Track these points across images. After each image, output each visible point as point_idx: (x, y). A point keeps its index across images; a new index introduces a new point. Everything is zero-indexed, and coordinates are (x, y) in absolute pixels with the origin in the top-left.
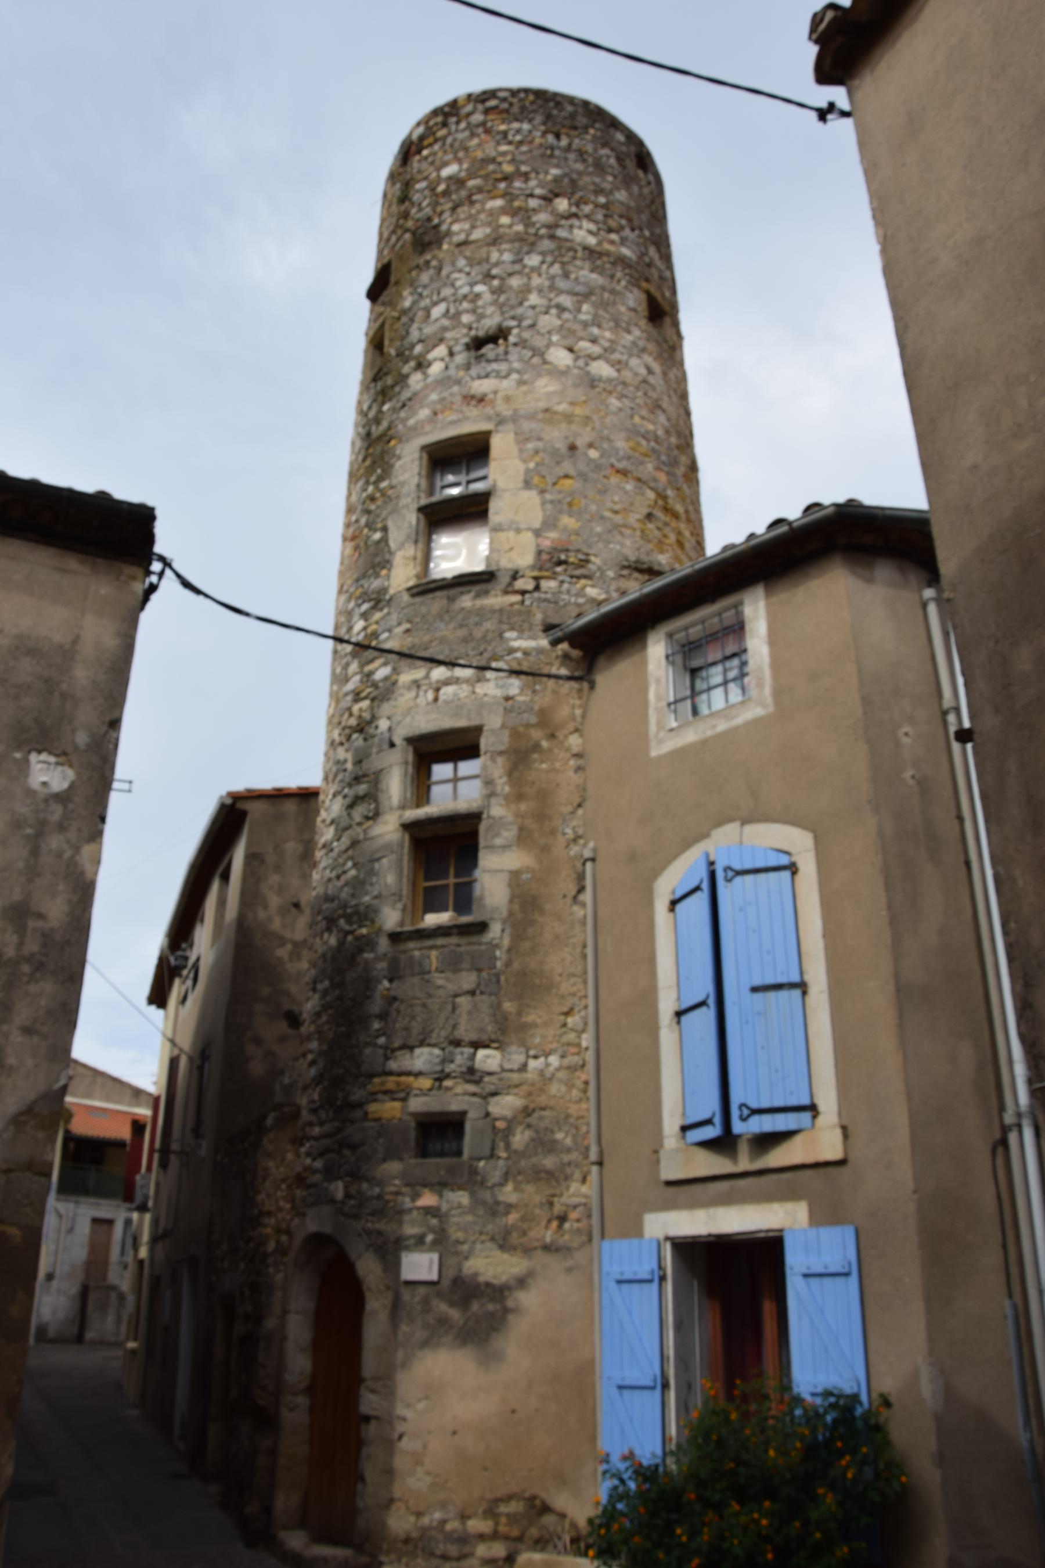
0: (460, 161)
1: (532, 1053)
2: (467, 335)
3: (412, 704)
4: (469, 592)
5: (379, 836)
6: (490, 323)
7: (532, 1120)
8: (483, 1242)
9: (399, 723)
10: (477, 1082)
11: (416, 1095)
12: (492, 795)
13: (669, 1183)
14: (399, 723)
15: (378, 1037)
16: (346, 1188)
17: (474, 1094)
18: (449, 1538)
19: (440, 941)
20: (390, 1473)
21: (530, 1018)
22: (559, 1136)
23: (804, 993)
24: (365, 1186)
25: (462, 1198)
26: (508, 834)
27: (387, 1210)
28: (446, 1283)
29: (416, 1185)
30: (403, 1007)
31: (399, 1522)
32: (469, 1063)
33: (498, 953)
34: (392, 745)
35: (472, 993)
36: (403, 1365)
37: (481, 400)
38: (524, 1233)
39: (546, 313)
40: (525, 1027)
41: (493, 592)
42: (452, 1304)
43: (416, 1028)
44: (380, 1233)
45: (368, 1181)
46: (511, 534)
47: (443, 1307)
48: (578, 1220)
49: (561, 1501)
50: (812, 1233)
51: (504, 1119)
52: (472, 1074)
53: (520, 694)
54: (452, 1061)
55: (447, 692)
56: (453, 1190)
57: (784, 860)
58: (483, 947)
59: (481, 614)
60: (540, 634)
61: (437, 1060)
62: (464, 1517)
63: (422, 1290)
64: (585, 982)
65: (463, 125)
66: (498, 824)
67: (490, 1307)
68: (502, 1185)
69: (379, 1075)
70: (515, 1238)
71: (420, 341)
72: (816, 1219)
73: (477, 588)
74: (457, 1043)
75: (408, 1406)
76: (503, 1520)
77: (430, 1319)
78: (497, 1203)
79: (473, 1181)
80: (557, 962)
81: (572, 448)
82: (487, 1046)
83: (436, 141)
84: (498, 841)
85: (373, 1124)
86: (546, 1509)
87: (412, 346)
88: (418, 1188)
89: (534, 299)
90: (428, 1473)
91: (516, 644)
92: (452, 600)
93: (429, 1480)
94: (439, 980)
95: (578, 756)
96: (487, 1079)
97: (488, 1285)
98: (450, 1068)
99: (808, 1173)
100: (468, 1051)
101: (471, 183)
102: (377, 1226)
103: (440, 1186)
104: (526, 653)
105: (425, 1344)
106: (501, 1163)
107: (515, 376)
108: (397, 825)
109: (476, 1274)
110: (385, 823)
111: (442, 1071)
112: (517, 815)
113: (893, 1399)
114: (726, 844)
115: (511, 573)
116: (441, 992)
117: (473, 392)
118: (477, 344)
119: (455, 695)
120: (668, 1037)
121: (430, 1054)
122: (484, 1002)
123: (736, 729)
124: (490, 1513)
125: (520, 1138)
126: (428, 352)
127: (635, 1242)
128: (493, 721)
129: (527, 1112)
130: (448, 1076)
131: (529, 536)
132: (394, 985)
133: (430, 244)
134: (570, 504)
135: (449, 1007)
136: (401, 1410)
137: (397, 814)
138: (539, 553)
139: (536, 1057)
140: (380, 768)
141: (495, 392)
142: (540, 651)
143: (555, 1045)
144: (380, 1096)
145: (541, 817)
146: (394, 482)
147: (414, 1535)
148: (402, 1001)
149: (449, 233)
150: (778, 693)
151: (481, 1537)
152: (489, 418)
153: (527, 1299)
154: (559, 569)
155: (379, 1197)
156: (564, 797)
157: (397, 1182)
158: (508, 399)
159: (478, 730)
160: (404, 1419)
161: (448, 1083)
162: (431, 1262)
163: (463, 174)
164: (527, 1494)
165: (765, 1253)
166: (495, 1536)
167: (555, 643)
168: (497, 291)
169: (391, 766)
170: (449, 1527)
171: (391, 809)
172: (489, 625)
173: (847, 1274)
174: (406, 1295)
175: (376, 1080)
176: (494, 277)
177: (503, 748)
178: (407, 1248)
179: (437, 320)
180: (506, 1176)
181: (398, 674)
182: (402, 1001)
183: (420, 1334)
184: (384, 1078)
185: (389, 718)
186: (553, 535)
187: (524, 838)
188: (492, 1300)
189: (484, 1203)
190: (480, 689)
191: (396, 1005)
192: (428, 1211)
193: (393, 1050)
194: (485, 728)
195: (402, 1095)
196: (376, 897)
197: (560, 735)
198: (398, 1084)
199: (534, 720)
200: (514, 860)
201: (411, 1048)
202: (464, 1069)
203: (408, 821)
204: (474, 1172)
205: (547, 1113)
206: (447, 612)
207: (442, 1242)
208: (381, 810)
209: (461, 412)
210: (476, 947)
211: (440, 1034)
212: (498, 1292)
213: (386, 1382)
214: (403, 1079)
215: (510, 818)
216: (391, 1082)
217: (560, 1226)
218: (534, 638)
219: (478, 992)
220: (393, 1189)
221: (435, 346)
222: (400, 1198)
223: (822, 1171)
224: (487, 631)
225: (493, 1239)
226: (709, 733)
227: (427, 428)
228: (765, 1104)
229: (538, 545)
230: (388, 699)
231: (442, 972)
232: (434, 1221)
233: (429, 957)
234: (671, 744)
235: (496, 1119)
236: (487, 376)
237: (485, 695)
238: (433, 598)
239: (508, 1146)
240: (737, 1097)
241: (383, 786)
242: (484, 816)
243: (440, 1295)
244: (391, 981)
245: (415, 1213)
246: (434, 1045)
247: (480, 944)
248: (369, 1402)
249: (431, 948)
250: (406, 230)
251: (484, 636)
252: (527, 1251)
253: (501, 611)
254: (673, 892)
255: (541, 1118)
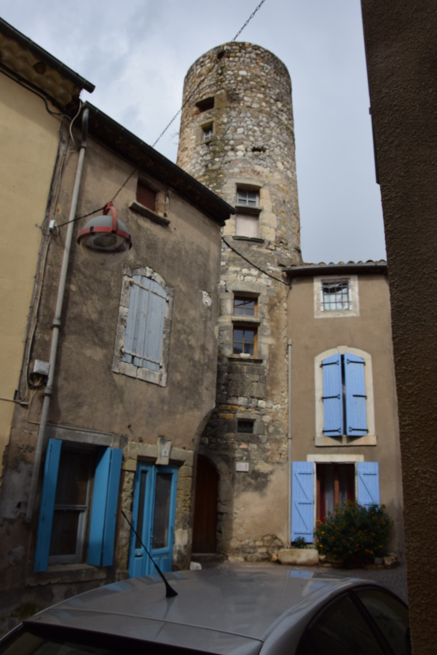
0: (247, 71)
1: (274, 403)
2: (251, 145)
3: (235, 279)
4: (256, 244)
5: (222, 322)
6: (260, 144)
7: (274, 424)
8: (260, 460)
9: (230, 284)
10: (259, 410)
11: (239, 412)
12: (264, 318)
13: (317, 447)
14: (230, 284)
15: (223, 391)
16: (209, 440)
17: (258, 414)
18: (251, 547)
19: (247, 363)
20: (231, 529)
21: (274, 392)
22: (280, 429)
23: (366, 399)
24: (219, 440)
25: (255, 446)
26: (268, 332)
27: (229, 448)
28: (250, 472)
29: (240, 441)
30: (234, 383)
31: (234, 544)
32: (256, 404)
33: (265, 370)
34: (227, 291)
35: (257, 382)
36: (237, 497)
37: (258, 173)
38: (272, 458)
39: (277, 147)
40: (273, 395)
41: (263, 247)
42: (252, 478)
43: (239, 391)
44: (226, 456)
45: (220, 438)
46: (268, 228)
47: (249, 479)
48: (284, 455)
49: (280, 536)
50: (366, 463)
51: (266, 423)
52: (257, 408)
53: (272, 285)
54: (251, 403)
55: (248, 278)
56: (252, 444)
57: (362, 361)
58: (261, 368)
59: (260, 253)
60: (277, 266)
61: (246, 402)
62: (255, 541)
63: (242, 474)
64: (288, 383)
65: (247, 56)
66: (265, 328)
67: (263, 480)
68: (266, 443)
69: (224, 404)
70: (270, 459)
71: (232, 139)
72: (366, 460)
73: (258, 244)
74: (253, 397)
75: (238, 509)
76: (265, 542)
77: (246, 483)
78: (265, 448)
79: (257, 441)
80: (281, 375)
81: (284, 202)
82: (261, 399)
83: (236, 56)
84: (266, 334)
85: (222, 420)
86: (276, 538)
87: (229, 140)
88: (240, 442)
89: (273, 140)
90: (244, 529)
91: (270, 268)
92: (250, 245)
93: (244, 531)
94: (247, 376)
95: (286, 310)
96: (262, 410)
97: (262, 473)
98: (251, 405)
99: (364, 448)
100: (256, 400)
101: (252, 83)
102: (225, 453)
103: (248, 442)
104: (273, 272)
105: (244, 490)
106: (266, 436)
107: (268, 169)
108: (230, 321)
109: (259, 470)
110: (225, 319)
111: (248, 406)
112: (271, 326)
113: (386, 506)
114: (353, 353)
115: (268, 242)
116: (248, 380)
117: (255, 169)
118: (254, 150)
119: (251, 280)
120: (319, 405)
121: (244, 400)
122: (261, 385)
123: (346, 318)
124: (262, 540)
125: (271, 429)
126: (237, 145)
127: (305, 463)
128: (264, 293)
129: (273, 421)
130: (250, 407)
131: (273, 230)
132: (230, 375)
133: (235, 100)
134: (284, 222)
135: (250, 385)
136: (235, 510)
137: (231, 317)
138: (276, 237)
139: (275, 405)
140: (223, 298)
141: (263, 172)
142: (277, 272)
143: (279, 402)
144: (225, 411)
145: (277, 328)
146: (223, 192)
147: (240, 547)
148: (233, 381)
149: (242, 99)
150: (361, 311)
151: (260, 547)
152: (261, 182)
153: (272, 478)
154: (281, 244)
155: (226, 444)
156: (283, 323)
157: (232, 440)
158: (267, 177)
159: (258, 294)
160: (236, 513)
161: (250, 410)
162: (246, 465)
163: (248, 77)
164: (272, 534)
165: (349, 469)
166: (263, 546)
167: (283, 271)
168: (263, 132)
169: (227, 299)
170: (250, 544)
171: (227, 314)
172: (262, 258)
173: (375, 475)
174: (237, 475)
175: (223, 406)
176: (261, 126)
177: (267, 303)
178: (237, 461)
179: (240, 134)
180: (267, 440)
181: (229, 266)
182: (233, 381)
183: (242, 488)
184: (226, 405)
185: (225, 281)
186: (280, 232)
187: (273, 334)
188: (264, 478)
189: (261, 448)
190: (260, 280)
191: (231, 382)
192: (244, 450)
193: (230, 397)
194: (261, 295)
195: (234, 412)
196: (221, 344)
197: (282, 301)
198: (232, 408)
199: (275, 295)
200: (270, 341)
201: (237, 397)
202: (255, 406)
203: (235, 320)
204: (258, 438)
205: (277, 422)
206: (248, 249)
207: (248, 459)
208: (223, 313)
209: (251, 176)
210: (259, 367)
211: (247, 394)
212: (265, 475)
213: (229, 501)
214: (233, 406)
215: (269, 327)
216: (229, 407)
217: (280, 457)
218: (275, 267)
219: (259, 382)
220: (231, 442)
221: (239, 144)
222: (234, 445)
223: (368, 447)
224: (262, 261)
225: (263, 459)
226: (337, 316)
227: (238, 177)
228: (356, 428)
229: (276, 234)
230: (224, 274)
231: (248, 373)
232: (246, 453)
233: (243, 368)
234: (322, 316)
235: (264, 423)
236: (260, 165)
237: (261, 283)
238: (243, 243)
239: (268, 431)
240: (349, 425)
241: (223, 305)
242: (261, 324)
243: (249, 476)
244: (229, 373)
245: (239, 450)
246: (245, 397)
247: (260, 366)
248: (222, 508)
249: (244, 365)
250: (223, 88)
251: (261, 262)
252: (273, 463)
253: (266, 254)
254: (322, 362)
255: (276, 423)
